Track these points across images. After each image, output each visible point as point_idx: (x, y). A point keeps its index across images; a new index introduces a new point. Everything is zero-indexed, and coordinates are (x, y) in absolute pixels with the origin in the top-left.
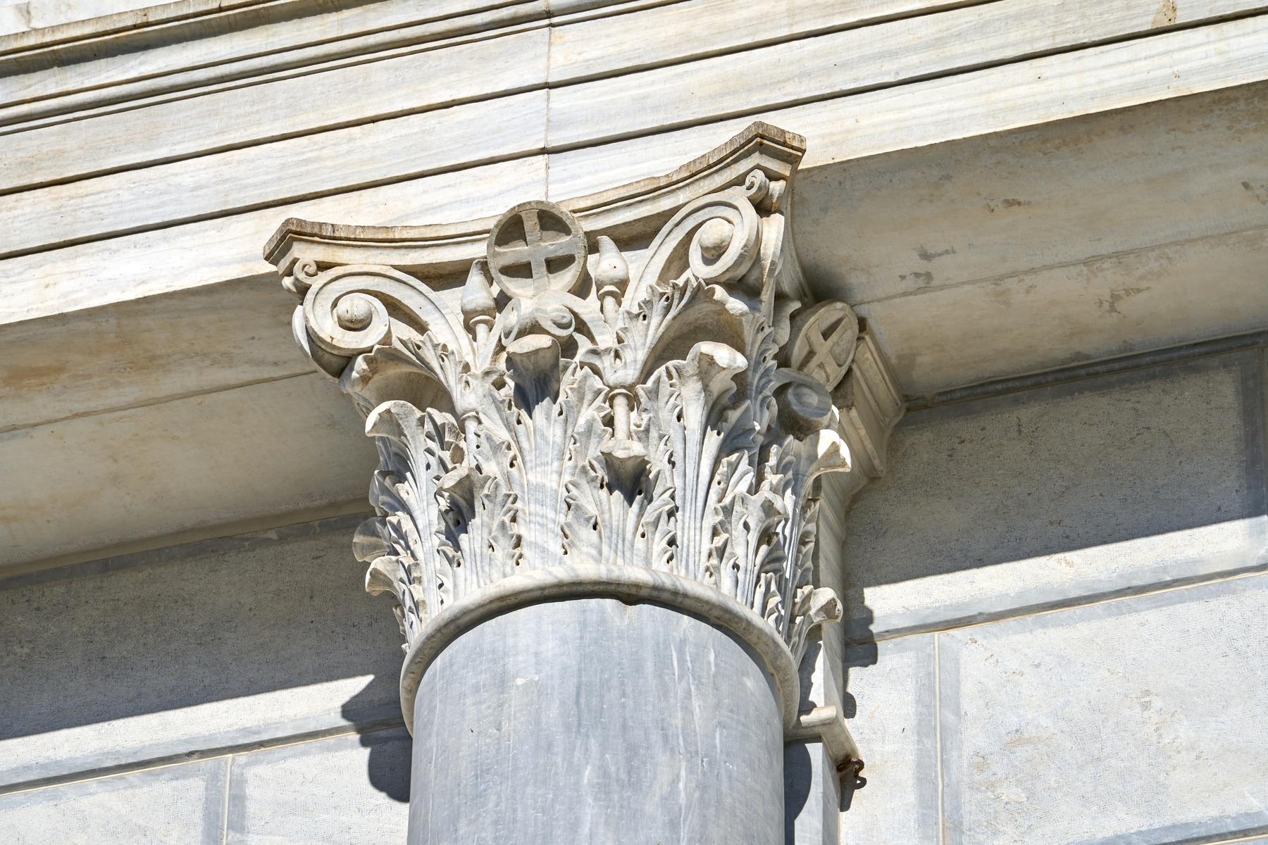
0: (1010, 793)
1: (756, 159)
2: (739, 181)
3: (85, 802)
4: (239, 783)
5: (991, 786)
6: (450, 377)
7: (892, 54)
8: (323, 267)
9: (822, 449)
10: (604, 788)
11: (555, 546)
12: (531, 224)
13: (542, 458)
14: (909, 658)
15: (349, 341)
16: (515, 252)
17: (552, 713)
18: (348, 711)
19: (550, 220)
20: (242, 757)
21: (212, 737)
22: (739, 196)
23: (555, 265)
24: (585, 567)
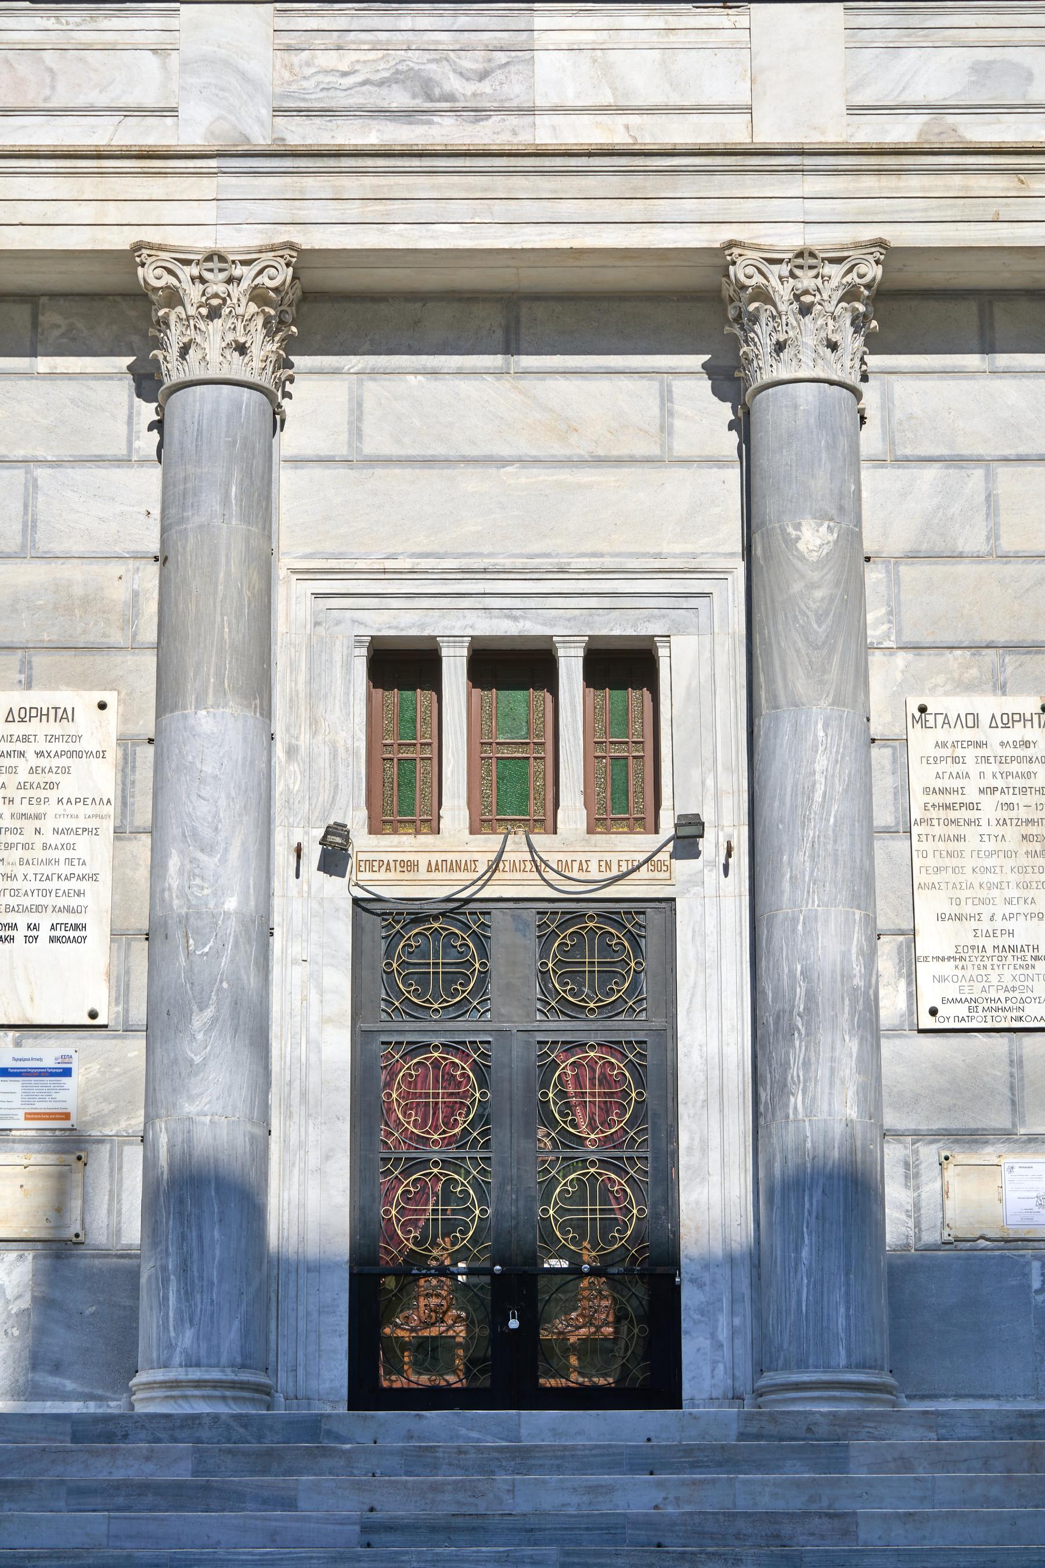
0: (909, 435)
1: (878, 249)
2: (872, 253)
3: (620, 383)
4: (669, 386)
5: (904, 431)
6: (777, 299)
7: (912, 211)
8: (740, 255)
9: (872, 326)
10: (827, 448)
11: (811, 364)
12: (806, 255)
13: (808, 334)
14: (878, 383)
15: (747, 282)
16: (800, 261)
17: (812, 421)
18: (704, 366)
19: (812, 255)
20: (670, 376)
21: (659, 368)
22: (870, 258)
23: (811, 267)
24: (822, 375)
